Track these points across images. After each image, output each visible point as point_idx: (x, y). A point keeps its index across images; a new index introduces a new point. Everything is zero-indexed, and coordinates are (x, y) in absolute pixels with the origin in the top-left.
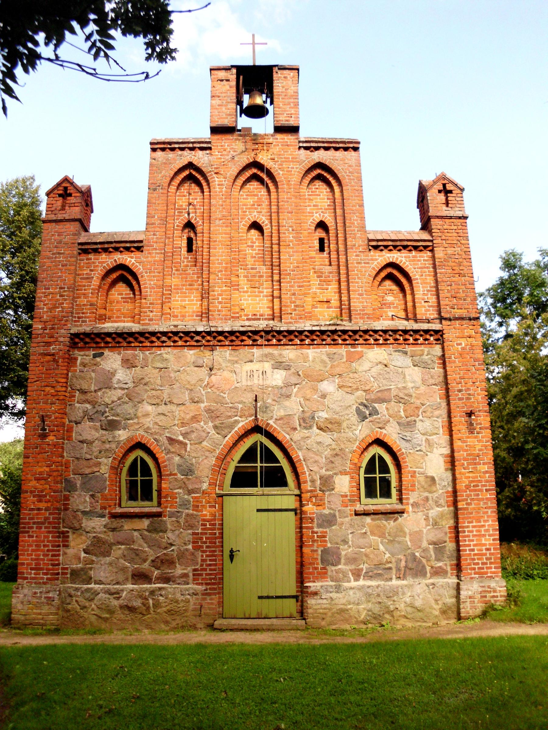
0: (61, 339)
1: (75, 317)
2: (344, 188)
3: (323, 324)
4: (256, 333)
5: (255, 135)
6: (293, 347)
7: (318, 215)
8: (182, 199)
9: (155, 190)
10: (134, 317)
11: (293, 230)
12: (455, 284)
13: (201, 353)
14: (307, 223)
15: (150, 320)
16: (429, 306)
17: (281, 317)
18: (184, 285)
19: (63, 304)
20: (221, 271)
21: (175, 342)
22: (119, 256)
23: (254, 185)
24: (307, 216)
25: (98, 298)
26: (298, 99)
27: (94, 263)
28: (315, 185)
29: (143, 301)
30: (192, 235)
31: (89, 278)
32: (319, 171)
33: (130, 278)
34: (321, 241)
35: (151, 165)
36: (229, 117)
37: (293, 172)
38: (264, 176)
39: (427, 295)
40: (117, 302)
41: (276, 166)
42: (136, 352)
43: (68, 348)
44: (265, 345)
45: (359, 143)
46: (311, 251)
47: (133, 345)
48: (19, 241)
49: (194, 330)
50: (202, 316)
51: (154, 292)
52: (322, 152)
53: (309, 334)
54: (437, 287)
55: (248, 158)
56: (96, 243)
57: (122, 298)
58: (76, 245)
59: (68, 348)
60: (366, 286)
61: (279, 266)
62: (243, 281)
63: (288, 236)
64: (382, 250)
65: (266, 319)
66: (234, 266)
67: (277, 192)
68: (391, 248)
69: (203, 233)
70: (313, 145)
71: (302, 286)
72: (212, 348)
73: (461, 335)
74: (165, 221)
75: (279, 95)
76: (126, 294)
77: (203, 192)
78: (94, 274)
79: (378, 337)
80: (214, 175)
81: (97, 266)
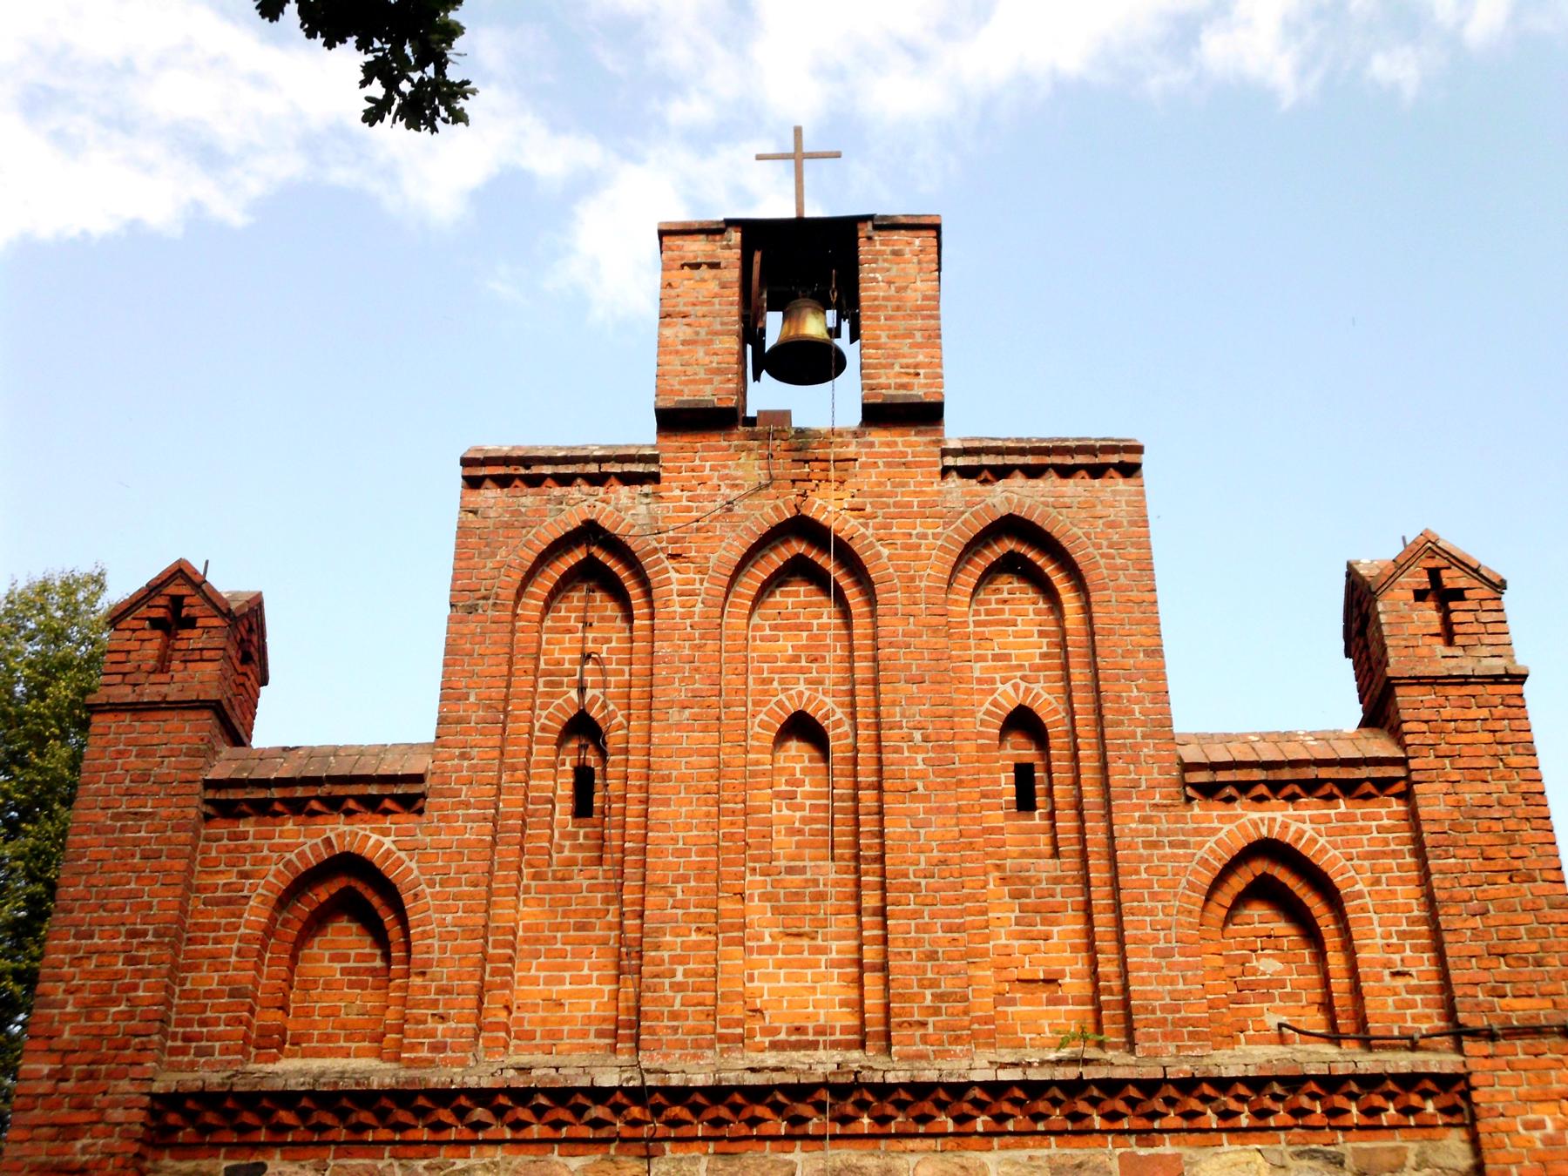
0: (117, 1115)
1: (174, 1036)
2: (1095, 597)
3: (1035, 1060)
4: (801, 1092)
5: (801, 432)
6: (930, 1142)
7: (1008, 687)
8: (560, 642)
9: (471, 609)
10: (380, 1038)
11: (925, 739)
12: (1501, 909)
13: (607, 1166)
14: (972, 714)
15: (435, 1048)
16: (1411, 990)
17: (887, 1036)
18: (556, 928)
19: (135, 987)
20: (686, 879)
21: (518, 1125)
22: (343, 828)
23: (798, 595)
24: (971, 692)
25: (258, 969)
26: (937, 318)
27: (253, 848)
28: (998, 591)
29: (417, 981)
30: (592, 759)
31: (234, 902)
32: (1009, 545)
33: (375, 901)
34: (1024, 775)
35: (463, 531)
36: (717, 379)
37: (923, 551)
38: (830, 565)
39: (1401, 949)
40: (328, 986)
41: (870, 532)
42: (380, 1164)
43: (136, 1147)
44: (834, 1137)
45: (1139, 450)
46: (990, 807)
47: (370, 1137)
48: (33, 783)
49: (584, 1082)
50: (615, 1035)
51: (455, 950)
52: (1017, 482)
53: (985, 1097)
54: (1433, 920)
55: (776, 508)
56: (265, 783)
57: (344, 971)
58: (199, 787)
59: (136, 1147)
60: (1179, 925)
61: (881, 859)
62: (758, 913)
63: (912, 761)
64: (1230, 800)
65: (835, 1045)
66: (728, 863)
67: (873, 614)
68: (1262, 790)
69: (626, 751)
70: (987, 460)
71: (960, 928)
72: (648, 1150)
73: (1537, 1092)
74: (501, 711)
75: (877, 308)
76: (361, 958)
77: (629, 618)
78: (254, 888)
79: (1233, 1105)
80: (667, 563)
81: (264, 860)
